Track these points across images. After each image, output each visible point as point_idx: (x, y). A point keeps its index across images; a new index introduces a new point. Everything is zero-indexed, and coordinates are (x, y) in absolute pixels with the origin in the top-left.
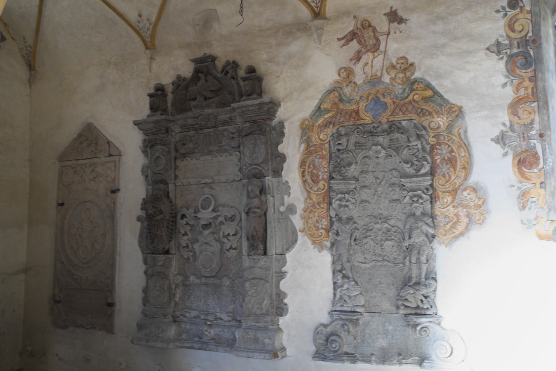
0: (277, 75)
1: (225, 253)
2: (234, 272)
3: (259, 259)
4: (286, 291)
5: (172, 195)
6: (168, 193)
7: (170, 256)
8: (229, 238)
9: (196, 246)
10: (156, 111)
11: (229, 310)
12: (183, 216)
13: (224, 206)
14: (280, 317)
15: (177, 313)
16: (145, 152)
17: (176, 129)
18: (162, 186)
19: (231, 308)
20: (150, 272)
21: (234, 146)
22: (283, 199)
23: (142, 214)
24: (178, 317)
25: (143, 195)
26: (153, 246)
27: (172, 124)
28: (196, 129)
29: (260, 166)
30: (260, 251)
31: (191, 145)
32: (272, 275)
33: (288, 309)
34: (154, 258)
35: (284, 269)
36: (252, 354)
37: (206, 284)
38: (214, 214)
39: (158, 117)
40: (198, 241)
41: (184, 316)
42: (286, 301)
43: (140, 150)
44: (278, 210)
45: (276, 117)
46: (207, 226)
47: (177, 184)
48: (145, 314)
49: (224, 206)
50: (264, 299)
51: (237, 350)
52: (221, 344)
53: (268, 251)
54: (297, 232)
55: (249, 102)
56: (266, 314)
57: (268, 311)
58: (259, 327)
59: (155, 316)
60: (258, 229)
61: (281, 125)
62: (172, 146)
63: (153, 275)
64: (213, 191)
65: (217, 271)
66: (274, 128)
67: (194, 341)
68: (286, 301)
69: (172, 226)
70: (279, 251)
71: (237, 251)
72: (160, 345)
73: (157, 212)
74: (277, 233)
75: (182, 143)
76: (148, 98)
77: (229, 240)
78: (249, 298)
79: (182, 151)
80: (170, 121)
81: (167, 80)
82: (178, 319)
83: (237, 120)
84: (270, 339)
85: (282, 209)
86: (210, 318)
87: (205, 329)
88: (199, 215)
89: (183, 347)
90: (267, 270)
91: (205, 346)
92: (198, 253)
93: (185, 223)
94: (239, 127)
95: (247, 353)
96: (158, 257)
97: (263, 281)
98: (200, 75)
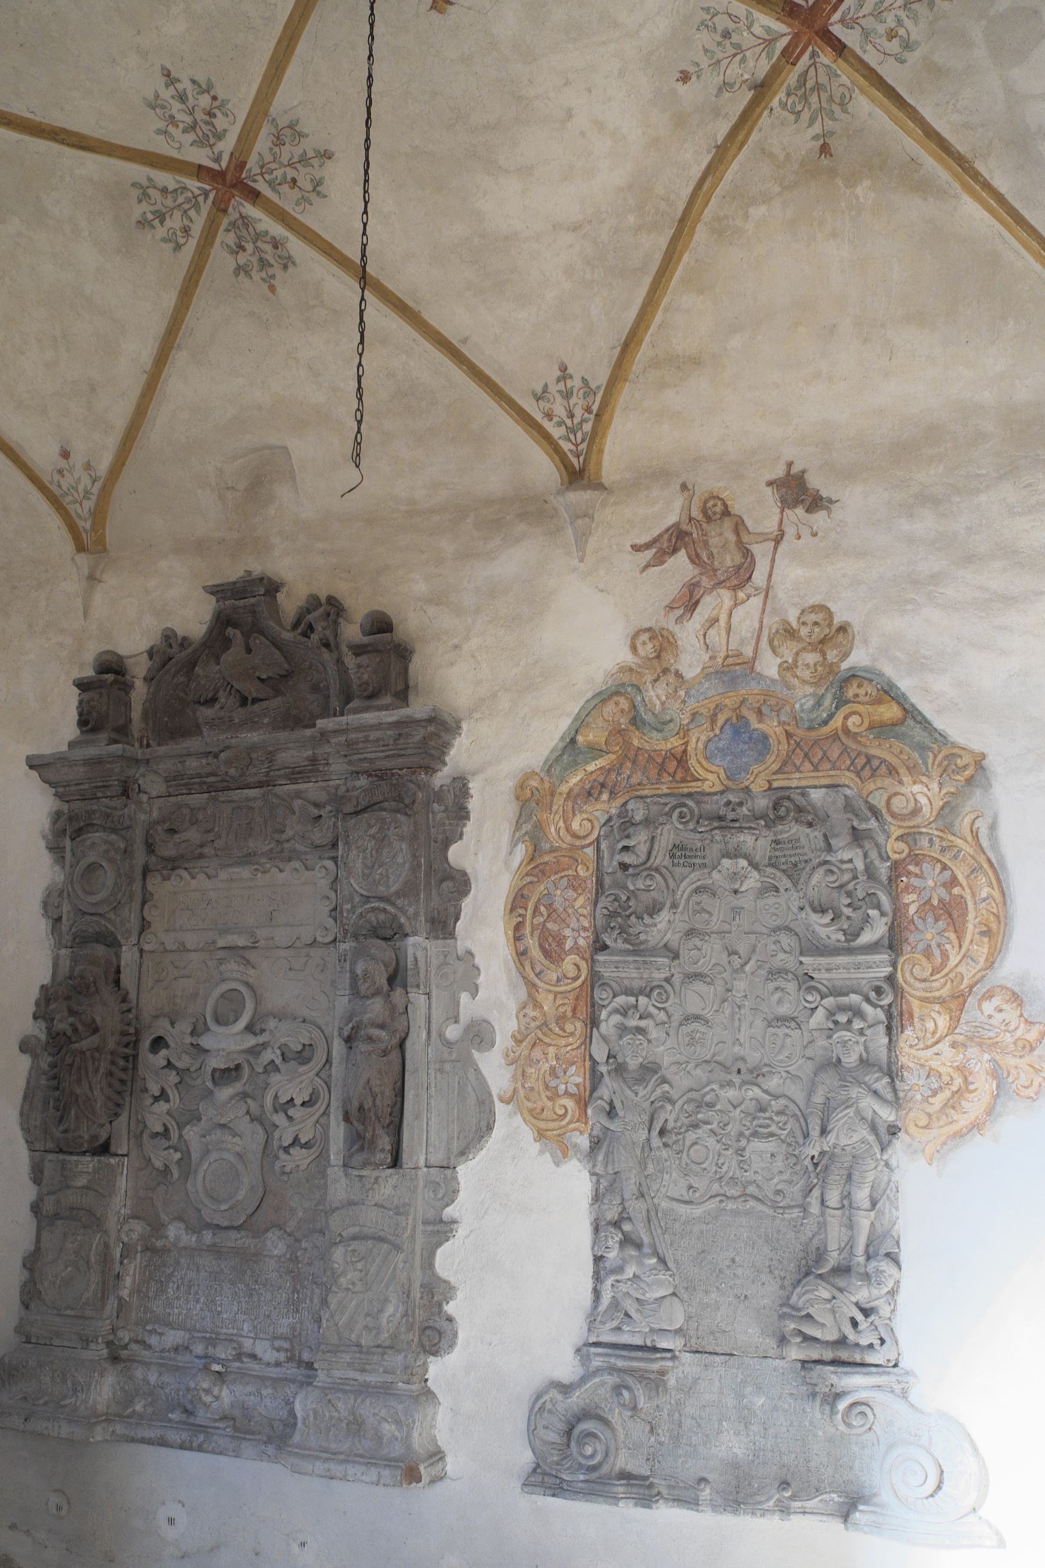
0: (456, 641)
1: (277, 1157)
2: (301, 1214)
3: (377, 1179)
5: (128, 979)
8: (290, 1113)
9: (191, 1134)
10: (94, 730)
12: (159, 1043)
14: (431, 1358)
15: (120, 1334)
16: (55, 849)
17: (153, 784)
18: (100, 950)
19: (284, 1324)
23: (37, 1032)
24: (125, 1347)
26: (61, 1128)
28: (211, 789)
30: (379, 1156)
31: (193, 835)
33: (455, 1335)
35: (449, 1212)
37: (215, 1250)
38: (251, 1041)
39: (101, 747)
42: (450, 1308)
43: (42, 844)
44: (441, 1035)
45: (445, 764)
50: (386, 1300)
52: (253, 1433)
54: (492, 1102)
55: (370, 717)
56: (391, 1347)
57: (395, 1336)
58: (366, 1385)
60: (377, 1090)
61: (461, 786)
62: (139, 835)
64: (251, 972)
66: (438, 796)
67: (170, 1420)
68: (450, 1308)
70: (437, 1157)
71: (314, 1152)
73: (80, 1028)
75: (166, 826)
76: (77, 691)
79: (168, 850)
81: (134, 642)
82: (124, 1354)
84: (398, 1422)
85: (452, 1032)
86: (223, 1352)
88: (206, 1041)
89: (133, 1440)
90: (398, 1213)
91: (202, 1437)
92: (195, 1156)
93: (165, 1063)
94: (337, 787)
95: (326, 1466)
96: (77, 1163)
98: (230, 631)
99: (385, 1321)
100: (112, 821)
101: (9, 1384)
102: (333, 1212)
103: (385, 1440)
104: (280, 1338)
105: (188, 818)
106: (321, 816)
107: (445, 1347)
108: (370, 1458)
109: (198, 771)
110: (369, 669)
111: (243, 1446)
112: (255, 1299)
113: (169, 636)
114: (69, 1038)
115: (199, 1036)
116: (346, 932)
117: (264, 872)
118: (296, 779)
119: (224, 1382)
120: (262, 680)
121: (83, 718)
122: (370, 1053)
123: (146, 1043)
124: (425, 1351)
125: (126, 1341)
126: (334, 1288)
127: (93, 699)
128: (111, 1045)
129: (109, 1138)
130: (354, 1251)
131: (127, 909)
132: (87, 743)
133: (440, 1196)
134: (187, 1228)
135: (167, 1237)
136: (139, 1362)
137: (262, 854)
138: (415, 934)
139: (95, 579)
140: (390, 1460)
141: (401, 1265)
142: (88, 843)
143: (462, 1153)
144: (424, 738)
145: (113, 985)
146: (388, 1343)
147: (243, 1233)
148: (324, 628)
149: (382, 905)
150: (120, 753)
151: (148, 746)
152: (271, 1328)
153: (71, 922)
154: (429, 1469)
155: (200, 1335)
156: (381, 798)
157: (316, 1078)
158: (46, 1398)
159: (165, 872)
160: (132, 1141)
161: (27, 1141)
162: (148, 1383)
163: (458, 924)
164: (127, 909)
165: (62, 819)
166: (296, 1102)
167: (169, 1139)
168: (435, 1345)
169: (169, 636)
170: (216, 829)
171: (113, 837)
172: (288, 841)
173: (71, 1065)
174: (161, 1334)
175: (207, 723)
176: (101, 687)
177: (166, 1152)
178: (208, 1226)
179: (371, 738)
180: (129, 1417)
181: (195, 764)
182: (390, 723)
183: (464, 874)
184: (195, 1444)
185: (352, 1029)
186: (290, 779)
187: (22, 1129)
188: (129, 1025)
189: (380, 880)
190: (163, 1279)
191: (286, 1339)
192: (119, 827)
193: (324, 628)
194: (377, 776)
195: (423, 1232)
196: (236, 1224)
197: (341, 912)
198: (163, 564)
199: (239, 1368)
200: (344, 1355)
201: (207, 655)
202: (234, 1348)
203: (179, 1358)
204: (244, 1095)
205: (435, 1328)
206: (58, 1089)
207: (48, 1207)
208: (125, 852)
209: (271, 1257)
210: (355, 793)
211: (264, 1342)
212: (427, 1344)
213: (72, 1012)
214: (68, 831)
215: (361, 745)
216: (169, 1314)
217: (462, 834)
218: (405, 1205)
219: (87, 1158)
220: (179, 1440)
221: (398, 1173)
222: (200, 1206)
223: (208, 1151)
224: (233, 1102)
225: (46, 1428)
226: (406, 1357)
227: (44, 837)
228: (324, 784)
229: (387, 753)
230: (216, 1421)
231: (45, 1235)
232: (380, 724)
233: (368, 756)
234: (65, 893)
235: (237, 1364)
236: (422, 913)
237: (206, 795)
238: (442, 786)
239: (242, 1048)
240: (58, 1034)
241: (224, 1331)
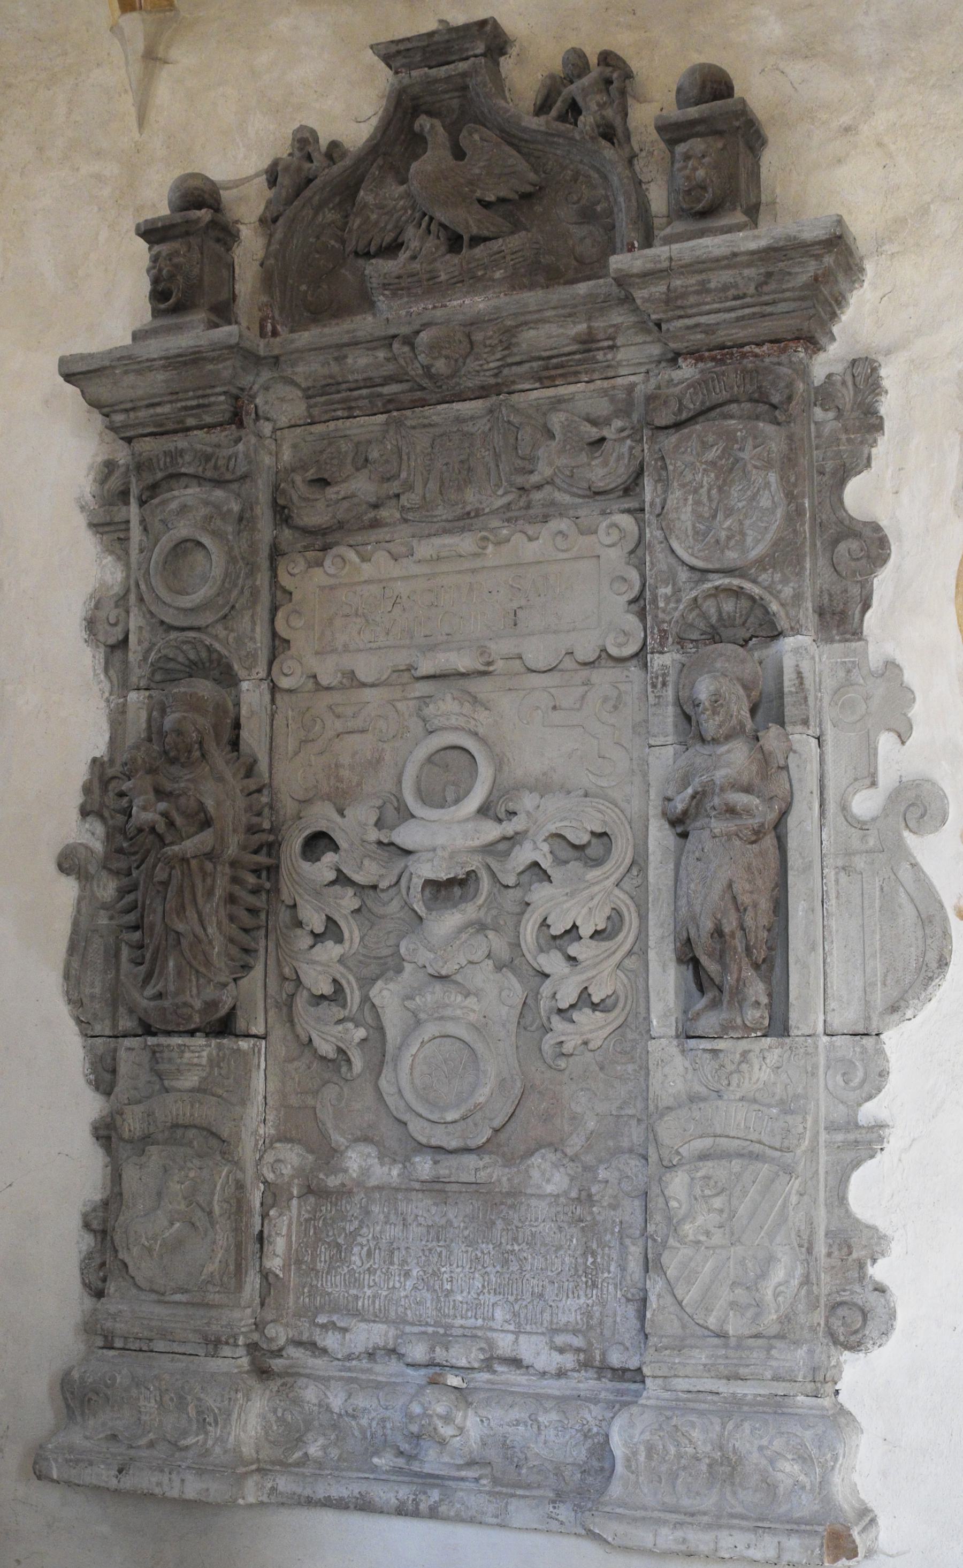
0: (845, 119)
1: (547, 1030)
2: (591, 1125)
3: (745, 1054)
4: (882, 1225)
5: (253, 737)
6: (237, 726)
7: (244, 1044)
8: (573, 950)
9: (386, 995)
10: (179, 309)
11: (563, 1319)
12: (319, 842)
13: (543, 787)
14: (847, 1355)
15: (271, 1331)
16: (108, 527)
17: (281, 404)
18: (204, 688)
19: (570, 1309)
20: (133, 1123)
21: (600, 485)
22: (872, 752)
23: (86, 839)
24: (278, 1353)
25: (93, 739)
26: (150, 991)
27: (266, 375)
28: (391, 405)
29: (754, 581)
30: (752, 1015)
31: (362, 486)
32: (816, 1135)
33: (893, 1316)
34: (154, 1052)
35: (869, 1112)
36: (708, 1537)
37: (436, 1188)
38: (491, 831)
39: (194, 334)
40: (399, 970)
41: (313, 1347)
42: (878, 1271)
43: (81, 521)
44: (844, 808)
45: (833, 339)
46: (446, 890)
47: (284, 683)
48: (101, 1336)
49: (543, 787)
50: (771, 1259)
51: (620, 1518)
52: (528, 1486)
53: (794, 1016)
54: (945, 919)
55: (712, 245)
56: (781, 1336)
57: (786, 1319)
58: (737, 1402)
59: (160, 1345)
60: (745, 899)
61: (865, 376)
62: (262, 493)
63: (146, 1140)
64: (482, 716)
65: (497, 1123)
66: (825, 395)
67: (374, 1469)
68: (878, 1271)
69: (255, 892)
70: (846, 1016)
71: (616, 1017)
72: (193, 1488)
73: (179, 820)
74: (833, 923)
75: (311, 474)
76: (142, 245)
77: (572, 959)
78: (686, 1251)
79: (315, 514)
80: (252, 359)
81: (238, 160)
82: (277, 1364)
83: (621, 355)
84: (804, 1459)
85: (865, 804)
86: (460, 1355)
87: (440, 1409)
88: (405, 836)
89: (310, 1502)
90: (787, 1112)
91: (435, 1495)
92: (393, 1034)
93: (332, 876)
94: (631, 389)
95: (679, 1534)
96: (182, 1049)
97: (765, 1169)
98: (424, 123)
99: (770, 1292)
100: (216, 468)
101: (83, 1414)
102: (662, 1116)
103: (781, 1490)
104: (564, 1330)
105: (349, 460)
106: (602, 440)
107: (875, 1334)
108: (760, 1520)
109: (370, 374)
110: (706, 160)
111: (511, 1508)
112: (514, 1267)
113: (304, 141)
114: (161, 838)
115: (392, 828)
116: (664, 634)
117: (498, 544)
118: (552, 378)
119: (469, 1404)
120: (486, 205)
121: (160, 288)
122: (729, 836)
123: (295, 843)
124: (836, 1342)
125: (282, 1341)
126: (671, 1242)
127: (176, 253)
128: (232, 850)
129: (234, 1008)
130: (707, 1178)
131: (247, 618)
132: (168, 330)
133: (856, 1081)
134: (381, 1157)
135: (346, 1171)
136: (308, 1376)
137: (492, 512)
138: (796, 631)
139: (156, 59)
140: (798, 1522)
141: (794, 1199)
142: (174, 505)
143: (894, 1009)
144: (816, 279)
145: (229, 748)
146: (774, 1330)
147: (487, 1159)
148: (601, 106)
149: (736, 582)
150: (233, 341)
151: (275, 333)
152: (547, 1316)
153: (146, 645)
154: (864, 1535)
155: (416, 1329)
156: (725, 395)
157: (617, 892)
158: (151, 1436)
159: (310, 554)
160: (271, 1013)
161: (79, 1022)
162: (329, 1409)
163: (868, 615)
164: (247, 618)
165: (117, 474)
166: (582, 932)
167: (344, 1006)
168: (856, 1332)
169: (304, 141)
170: (404, 475)
171: (219, 494)
172: (539, 487)
173: (166, 884)
174: (345, 1330)
175: (385, 286)
176: (187, 234)
177: (340, 1028)
178: (422, 1148)
179: (712, 285)
180: (297, 1464)
181: (363, 361)
182: (753, 253)
183: (877, 528)
184: (423, 1507)
185: (693, 797)
186: (540, 379)
187: (70, 1001)
188: (259, 814)
189: (729, 538)
190: (341, 1241)
191: (575, 1332)
192: (228, 476)
193: (601, 106)
194: (713, 359)
195: (828, 1145)
196: (472, 1144)
197: (655, 600)
198: (282, 24)
199: (488, 1381)
200: (695, 1353)
201: (381, 167)
202: (481, 1349)
203: (378, 1368)
204: (481, 927)
205: (855, 1305)
206: (136, 928)
207: (133, 1123)
208: (241, 519)
209: (540, 1197)
210: (677, 390)
211: (534, 1338)
212: (841, 1330)
213: (160, 793)
214: (127, 497)
215: (692, 299)
216: (357, 1298)
217: (869, 459)
218: (797, 1097)
219: (199, 1041)
220: (393, 1501)
221: (782, 1045)
222: (405, 1117)
223: (418, 1023)
224: (464, 936)
225: (159, 1484)
226: (811, 1352)
227: (82, 508)
228: (606, 384)
229: (740, 313)
230: (459, 1467)
231: (130, 1174)
232: (735, 255)
233: (703, 319)
234: (133, 597)
235: (486, 1376)
236: (808, 594)
237: (384, 416)
238: (829, 376)
239: (477, 843)
240: (140, 830)
241: (459, 1322)
